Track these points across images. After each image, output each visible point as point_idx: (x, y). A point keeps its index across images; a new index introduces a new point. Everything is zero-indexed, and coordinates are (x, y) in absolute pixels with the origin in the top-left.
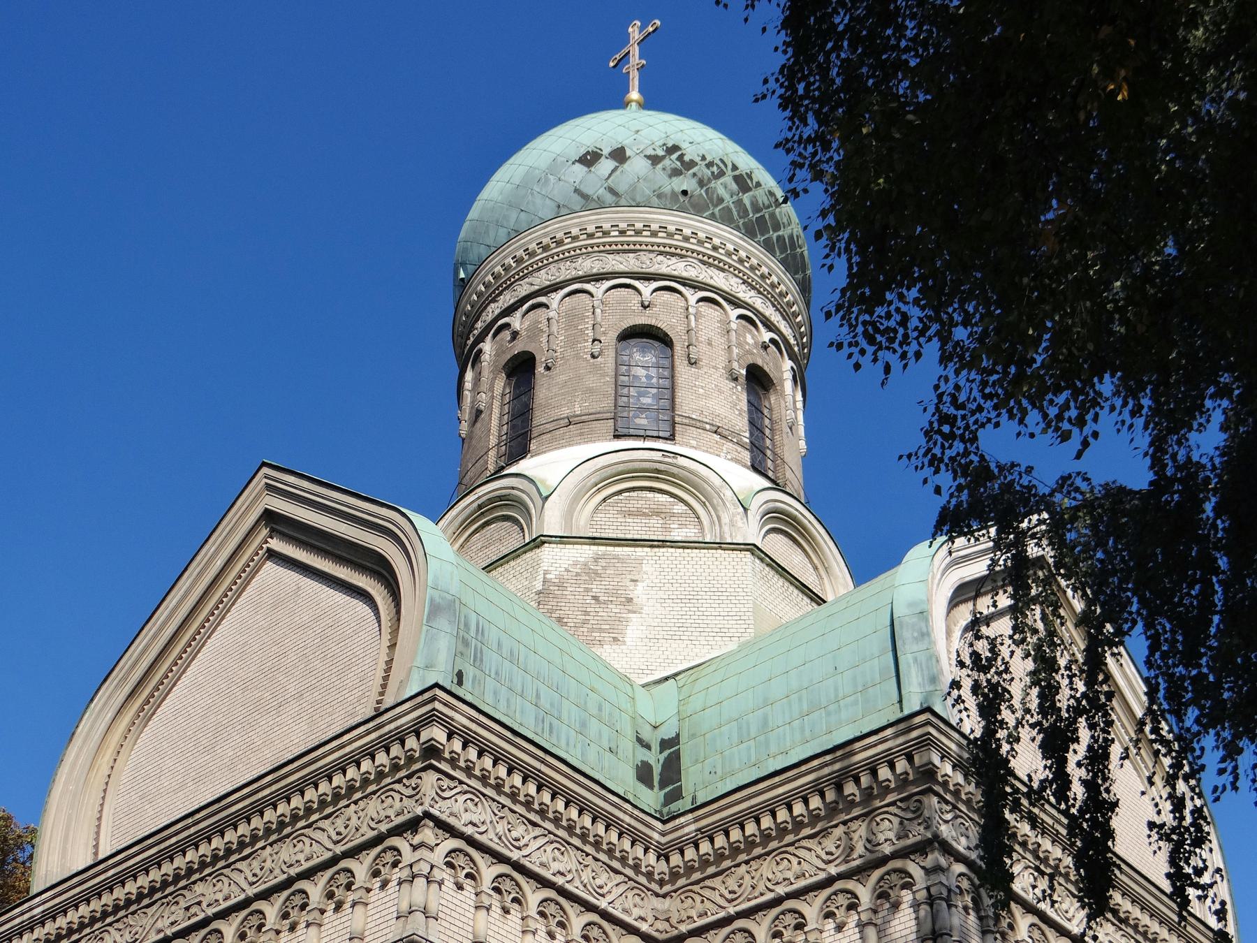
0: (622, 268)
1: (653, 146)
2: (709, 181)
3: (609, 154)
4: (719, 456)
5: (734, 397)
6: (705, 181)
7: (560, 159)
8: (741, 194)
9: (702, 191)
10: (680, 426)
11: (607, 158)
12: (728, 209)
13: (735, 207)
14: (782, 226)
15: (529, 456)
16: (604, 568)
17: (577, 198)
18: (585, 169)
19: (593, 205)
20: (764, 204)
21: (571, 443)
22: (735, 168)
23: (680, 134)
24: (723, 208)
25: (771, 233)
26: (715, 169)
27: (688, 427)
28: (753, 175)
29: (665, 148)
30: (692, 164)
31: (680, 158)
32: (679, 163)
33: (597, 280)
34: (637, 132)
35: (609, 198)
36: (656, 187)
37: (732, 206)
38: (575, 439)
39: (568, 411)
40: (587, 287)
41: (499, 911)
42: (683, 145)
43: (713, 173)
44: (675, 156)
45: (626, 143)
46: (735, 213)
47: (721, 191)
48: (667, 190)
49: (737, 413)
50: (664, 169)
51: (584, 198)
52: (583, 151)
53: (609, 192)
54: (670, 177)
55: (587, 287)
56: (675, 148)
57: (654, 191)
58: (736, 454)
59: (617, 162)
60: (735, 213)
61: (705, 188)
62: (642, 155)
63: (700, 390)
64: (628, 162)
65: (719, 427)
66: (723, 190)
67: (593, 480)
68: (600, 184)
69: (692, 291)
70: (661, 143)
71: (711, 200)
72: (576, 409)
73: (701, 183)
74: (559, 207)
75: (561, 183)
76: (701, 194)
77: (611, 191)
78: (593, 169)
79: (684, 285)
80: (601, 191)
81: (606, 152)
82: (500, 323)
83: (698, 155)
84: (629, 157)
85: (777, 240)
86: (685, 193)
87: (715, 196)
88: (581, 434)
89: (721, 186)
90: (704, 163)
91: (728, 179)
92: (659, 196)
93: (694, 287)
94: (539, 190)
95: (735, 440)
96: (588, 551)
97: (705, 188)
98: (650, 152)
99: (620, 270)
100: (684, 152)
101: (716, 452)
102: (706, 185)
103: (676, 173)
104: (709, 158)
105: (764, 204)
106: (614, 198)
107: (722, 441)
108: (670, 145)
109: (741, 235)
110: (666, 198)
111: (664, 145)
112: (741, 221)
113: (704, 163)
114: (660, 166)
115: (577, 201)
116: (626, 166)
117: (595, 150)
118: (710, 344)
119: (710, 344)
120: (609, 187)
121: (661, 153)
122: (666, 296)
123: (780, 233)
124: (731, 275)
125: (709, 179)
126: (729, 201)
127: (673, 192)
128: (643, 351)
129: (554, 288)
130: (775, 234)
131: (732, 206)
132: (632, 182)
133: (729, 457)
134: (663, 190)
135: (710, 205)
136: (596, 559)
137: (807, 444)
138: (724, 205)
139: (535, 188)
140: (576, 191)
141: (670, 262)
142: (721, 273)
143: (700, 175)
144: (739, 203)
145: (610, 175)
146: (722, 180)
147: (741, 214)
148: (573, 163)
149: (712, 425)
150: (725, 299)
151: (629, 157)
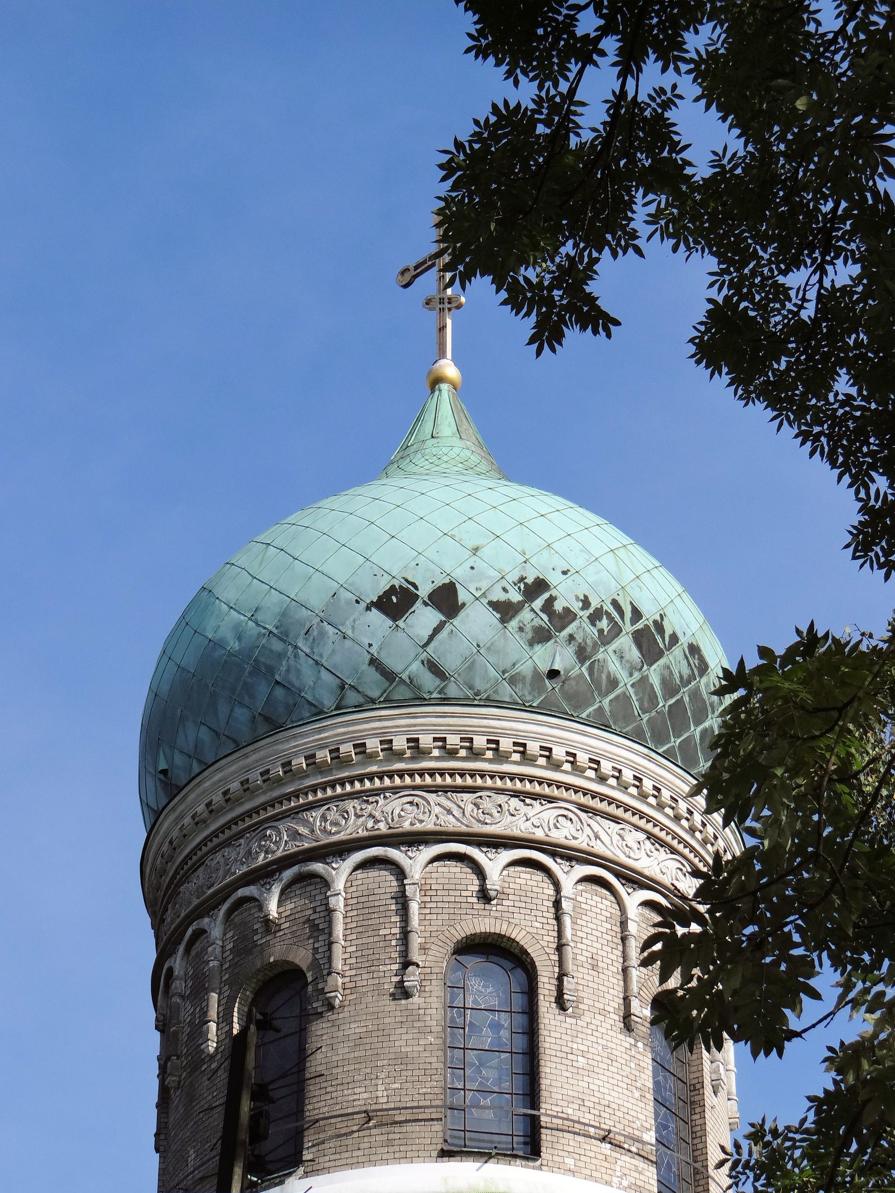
0: (450, 824)
1: (504, 583)
2: (595, 646)
3: (430, 596)
4: (608, 1183)
5: (633, 1065)
6: (589, 650)
7: (346, 596)
8: (645, 667)
9: (583, 669)
10: (548, 1132)
11: (426, 604)
12: (625, 698)
13: (636, 694)
14: (710, 709)
15: (301, 1170)
17: (373, 675)
18: (390, 622)
19: (402, 693)
20: (681, 677)
21: (373, 1158)
22: (637, 614)
23: (545, 553)
24: (617, 697)
25: (692, 728)
26: (604, 624)
27: (560, 1134)
28: (666, 623)
29: (522, 586)
30: (568, 616)
31: (548, 606)
32: (545, 617)
33: (410, 844)
34: (476, 549)
35: (429, 681)
36: (507, 664)
38: (380, 1150)
39: (365, 1096)
40: (393, 853)
42: (554, 578)
43: (601, 631)
44: (538, 603)
45: (459, 574)
47: (615, 667)
48: (525, 668)
49: (637, 1094)
50: (521, 629)
51: (387, 679)
52: (384, 585)
53: (430, 669)
54: (531, 644)
55: (393, 853)
56: (540, 585)
57: (504, 672)
58: (637, 1175)
59: (443, 614)
61: (588, 664)
62: (485, 601)
63: (581, 1059)
64: (462, 615)
65: (609, 1131)
66: (617, 664)
68: (413, 655)
69: (565, 865)
70: (514, 577)
71: (597, 683)
72: (380, 1094)
73: (582, 654)
74: (342, 687)
75: (348, 643)
76: (582, 674)
77: (434, 668)
78: (401, 623)
79: (553, 855)
80: (416, 667)
81: (424, 591)
82: (242, 892)
83: (577, 598)
84: (464, 605)
86: (553, 674)
87: (604, 676)
88: (389, 1143)
89: (614, 658)
90: (587, 613)
91: (625, 642)
92: (513, 681)
93: (569, 859)
94: (308, 651)
95: (634, 1149)
97: (588, 664)
98: (498, 595)
99: (450, 828)
100: (554, 592)
101: (605, 1177)
102: (590, 658)
103: (541, 636)
104: (595, 603)
105: (681, 677)
106: (438, 681)
107: (614, 1154)
108: (530, 580)
109: (646, 751)
110: (524, 684)
111: (522, 579)
112: (645, 717)
113: (587, 613)
114: (514, 624)
115: (373, 684)
116: (456, 621)
117: (405, 585)
118: (594, 967)
119: (594, 967)
120: (429, 661)
121: (515, 597)
122: (526, 875)
123: (706, 724)
124: (628, 827)
125: (595, 645)
126: (626, 681)
127: (536, 673)
128: (482, 975)
129: (342, 849)
130: (699, 729)
132: (468, 653)
133: (625, 1183)
134: (519, 668)
135: (596, 694)
138: (618, 691)
139: (300, 645)
140: (374, 662)
141: (531, 812)
142: (613, 824)
143: (579, 638)
144: (643, 684)
145: (431, 638)
146: (615, 645)
147: (646, 705)
148: (368, 608)
149: (599, 1128)
150: (618, 875)
151: (464, 605)
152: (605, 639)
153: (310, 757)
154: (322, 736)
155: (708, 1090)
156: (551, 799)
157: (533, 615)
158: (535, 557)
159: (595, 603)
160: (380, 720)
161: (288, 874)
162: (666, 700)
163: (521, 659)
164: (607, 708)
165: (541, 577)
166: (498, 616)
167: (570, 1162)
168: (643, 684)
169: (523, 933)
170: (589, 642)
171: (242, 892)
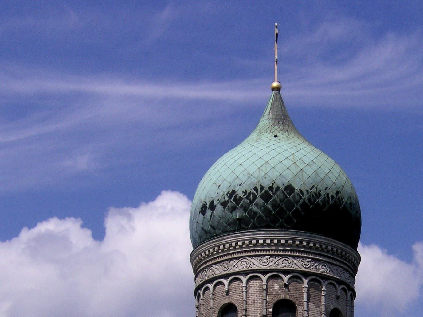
2: (249, 205)
12: (260, 216)
19: (209, 236)
24: (258, 217)
30: (241, 198)
47: (255, 209)
98: (223, 200)
103: (233, 209)
118: (253, 303)
121: (227, 199)
151: (216, 205)
152: (251, 202)
154: (342, 247)
157: (231, 203)
158: (248, 168)
160: (221, 240)
161: (215, 282)
162: (275, 211)
163: (230, 217)
164: (255, 222)
165: (234, 189)
166: (223, 207)
168: (266, 210)
169: (292, 297)
170: (247, 205)
171: (206, 286)
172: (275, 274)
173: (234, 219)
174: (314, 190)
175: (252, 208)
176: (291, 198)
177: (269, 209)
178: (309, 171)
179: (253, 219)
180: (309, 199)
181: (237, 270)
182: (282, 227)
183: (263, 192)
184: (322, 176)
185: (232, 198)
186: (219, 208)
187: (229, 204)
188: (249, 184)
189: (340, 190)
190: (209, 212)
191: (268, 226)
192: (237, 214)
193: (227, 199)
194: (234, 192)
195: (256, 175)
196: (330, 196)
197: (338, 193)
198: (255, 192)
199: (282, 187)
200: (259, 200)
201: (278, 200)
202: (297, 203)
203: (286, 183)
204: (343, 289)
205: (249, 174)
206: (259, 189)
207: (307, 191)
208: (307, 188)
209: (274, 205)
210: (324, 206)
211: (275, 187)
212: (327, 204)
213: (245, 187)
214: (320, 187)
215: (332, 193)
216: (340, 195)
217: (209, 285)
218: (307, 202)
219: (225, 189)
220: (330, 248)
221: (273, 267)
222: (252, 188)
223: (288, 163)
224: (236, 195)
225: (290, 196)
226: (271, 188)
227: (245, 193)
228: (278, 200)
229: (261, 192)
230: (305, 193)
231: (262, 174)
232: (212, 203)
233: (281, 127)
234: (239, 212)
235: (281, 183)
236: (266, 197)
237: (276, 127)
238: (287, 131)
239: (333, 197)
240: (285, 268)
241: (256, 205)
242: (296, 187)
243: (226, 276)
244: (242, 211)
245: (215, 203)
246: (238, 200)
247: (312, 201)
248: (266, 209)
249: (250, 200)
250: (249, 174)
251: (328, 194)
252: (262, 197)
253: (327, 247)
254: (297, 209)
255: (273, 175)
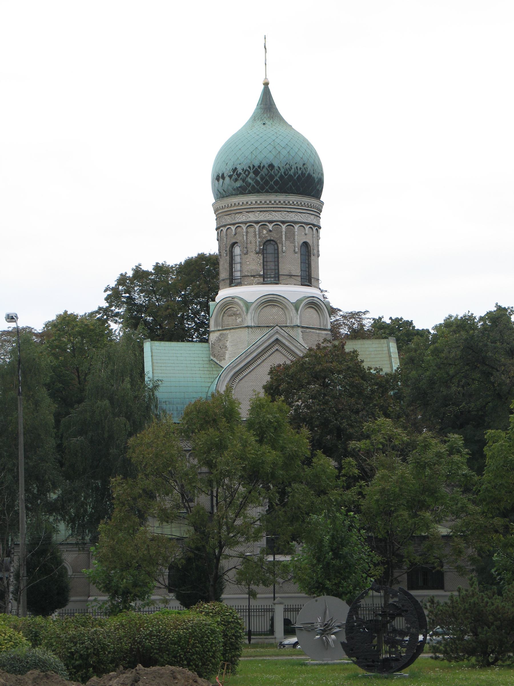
2: (246, 179)
12: (253, 185)
16: (222, 338)
26: (247, 173)
30: (240, 174)
37: (254, 184)
41: (195, 683)
46: (256, 186)
47: (250, 181)
54: (235, 182)
60: (256, 186)
67: (220, 309)
85: (279, 179)
96: (219, 333)
98: (229, 174)
103: (236, 180)
104: (245, 169)
118: (251, 243)
121: (232, 173)
130: (399, 472)
131: (254, 184)
136: (220, 335)
137: (423, 613)
138: (252, 185)
152: (247, 176)
153: (293, 202)
155: (312, 255)
156: (241, 213)
159: (245, 169)
162: (262, 181)
167: (246, 283)
168: (257, 182)
172: (263, 224)
173: (237, 187)
174: (288, 166)
175: (248, 180)
176: (272, 173)
177: (258, 181)
178: (284, 152)
179: (249, 187)
180: (285, 173)
181: (240, 221)
182: (267, 192)
183: (254, 169)
184: (293, 155)
185: (235, 173)
186: (227, 179)
187: (233, 177)
188: (246, 164)
189: (306, 163)
190: (221, 181)
191: (258, 192)
192: (239, 184)
193: (232, 173)
194: (236, 169)
195: (250, 157)
196: (298, 168)
197: (304, 164)
198: (249, 170)
199: (266, 166)
200: (252, 175)
201: (264, 174)
202: (276, 175)
203: (269, 163)
204: (310, 227)
205: (245, 156)
206: (252, 168)
207: (283, 167)
208: (283, 165)
209: (262, 178)
210: (295, 175)
211: (262, 165)
212: (296, 174)
213: (243, 166)
214: (291, 163)
215: (300, 165)
216: (305, 166)
217: (232, 227)
218: (283, 174)
219: (230, 167)
220: (299, 203)
221: (262, 219)
222: (247, 166)
223: (270, 148)
224: (238, 171)
225: (271, 171)
226: (259, 167)
227: (243, 170)
228: (264, 174)
229: (253, 169)
230: (281, 168)
231: (254, 157)
232: (223, 175)
233: (269, 115)
234: (62, 446)
235: (265, 163)
236: (256, 173)
237: (265, 115)
238: (272, 118)
239: (300, 168)
240: (270, 219)
241: (250, 178)
242: (276, 165)
243: (234, 224)
244: (241, 181)
245: (225, 175)
246: (239, 175)
247: (286, 173)
248: (257, 181)
249: (246, 175)
250: (245, 156)
251: (297, 167)
252: (254, 173)
253: (293, 202)
254: (267, 186)
255: (260, 157)
